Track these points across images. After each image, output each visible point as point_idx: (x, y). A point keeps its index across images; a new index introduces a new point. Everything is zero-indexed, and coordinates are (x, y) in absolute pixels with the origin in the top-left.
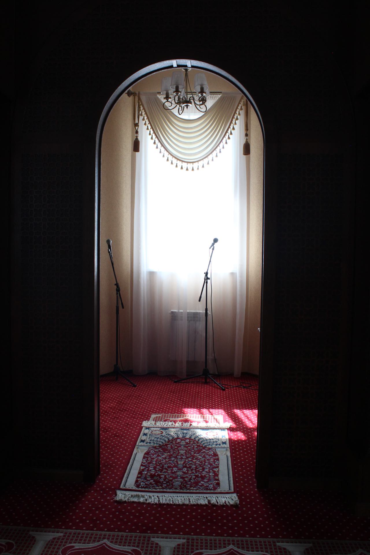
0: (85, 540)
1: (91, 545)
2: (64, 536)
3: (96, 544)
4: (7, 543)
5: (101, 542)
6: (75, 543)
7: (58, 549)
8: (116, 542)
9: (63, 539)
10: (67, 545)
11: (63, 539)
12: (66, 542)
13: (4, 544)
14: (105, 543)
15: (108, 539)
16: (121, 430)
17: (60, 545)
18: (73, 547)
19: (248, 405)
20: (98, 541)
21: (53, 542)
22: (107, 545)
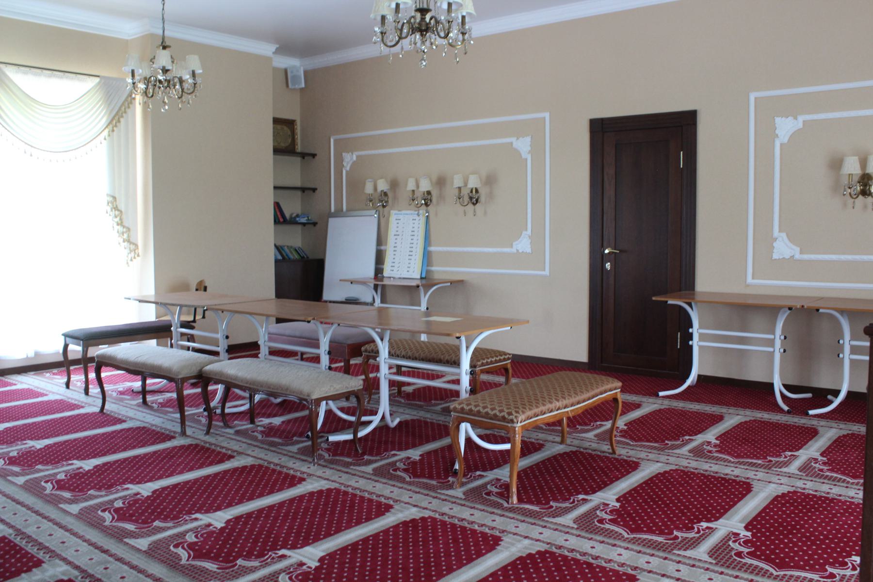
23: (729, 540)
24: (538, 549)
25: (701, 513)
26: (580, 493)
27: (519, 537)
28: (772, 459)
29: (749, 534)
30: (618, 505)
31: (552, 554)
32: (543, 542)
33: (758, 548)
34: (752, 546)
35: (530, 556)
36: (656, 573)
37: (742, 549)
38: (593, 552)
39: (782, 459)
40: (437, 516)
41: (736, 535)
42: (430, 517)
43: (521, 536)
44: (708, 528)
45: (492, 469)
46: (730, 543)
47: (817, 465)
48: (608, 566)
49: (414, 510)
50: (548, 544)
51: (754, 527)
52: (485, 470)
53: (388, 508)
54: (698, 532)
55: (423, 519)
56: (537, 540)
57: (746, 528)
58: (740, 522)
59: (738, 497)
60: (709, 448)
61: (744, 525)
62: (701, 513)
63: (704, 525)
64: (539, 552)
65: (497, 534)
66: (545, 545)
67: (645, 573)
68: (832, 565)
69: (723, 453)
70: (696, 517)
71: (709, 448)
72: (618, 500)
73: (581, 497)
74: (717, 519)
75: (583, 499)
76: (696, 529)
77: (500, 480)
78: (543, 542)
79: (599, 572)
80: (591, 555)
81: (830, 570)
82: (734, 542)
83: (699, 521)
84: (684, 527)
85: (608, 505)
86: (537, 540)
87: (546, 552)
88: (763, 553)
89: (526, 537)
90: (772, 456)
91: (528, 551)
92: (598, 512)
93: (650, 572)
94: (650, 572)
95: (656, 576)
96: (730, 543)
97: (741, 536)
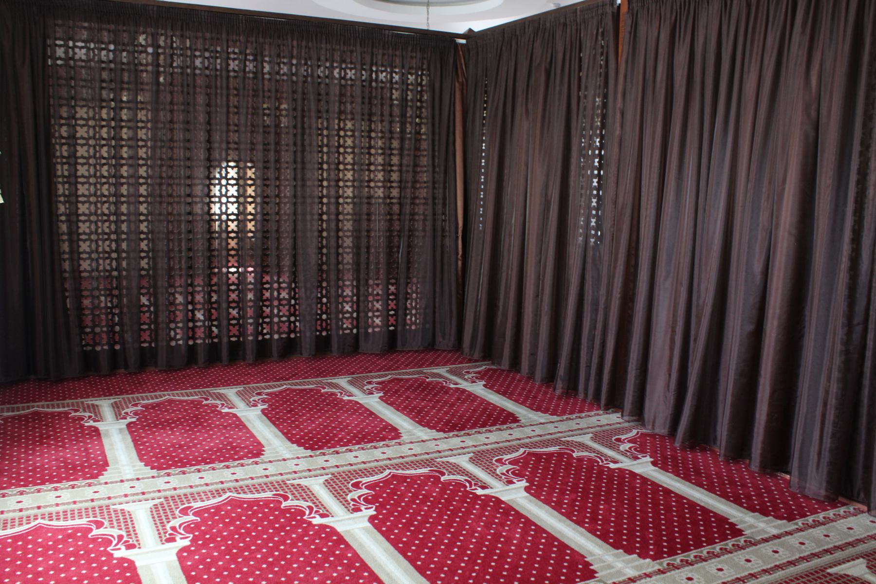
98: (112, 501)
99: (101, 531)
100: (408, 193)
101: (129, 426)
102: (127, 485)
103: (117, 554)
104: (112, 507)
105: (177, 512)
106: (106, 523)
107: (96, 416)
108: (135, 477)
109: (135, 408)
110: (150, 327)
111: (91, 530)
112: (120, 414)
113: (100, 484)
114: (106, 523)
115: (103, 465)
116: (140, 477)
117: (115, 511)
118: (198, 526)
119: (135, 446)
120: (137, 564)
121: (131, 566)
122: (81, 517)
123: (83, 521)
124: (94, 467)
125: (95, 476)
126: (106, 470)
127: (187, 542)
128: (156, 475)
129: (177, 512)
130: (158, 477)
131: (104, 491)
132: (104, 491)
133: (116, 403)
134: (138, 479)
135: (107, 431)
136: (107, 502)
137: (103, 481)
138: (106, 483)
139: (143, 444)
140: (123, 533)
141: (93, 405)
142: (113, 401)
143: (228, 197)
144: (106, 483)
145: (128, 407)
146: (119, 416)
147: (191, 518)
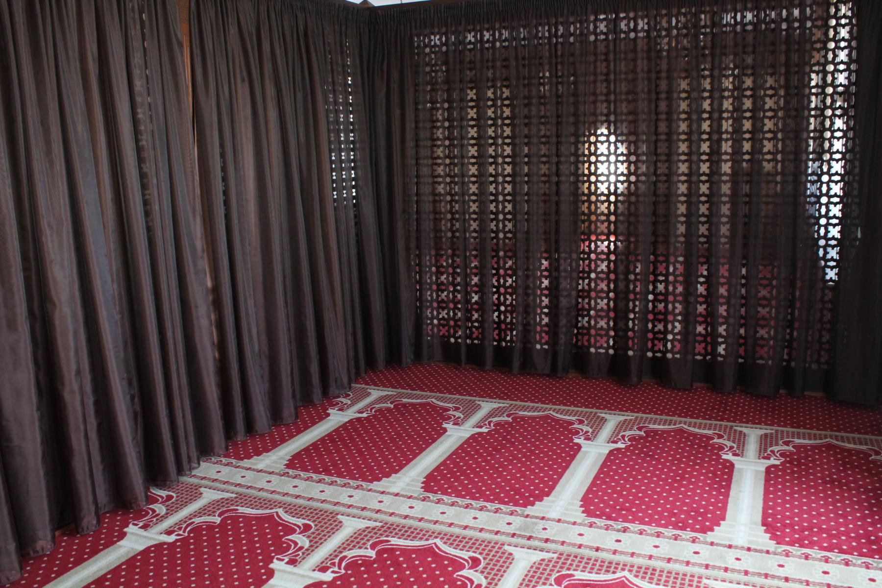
0: (458, 545)
1: (254, 512)
2: (559, 558)
3: (610, 576)
4: (305, 525)
5: (430, 542)
6: (575, 570)
7: (550, 575)
8: (644, 578)
9: (379, 530)
10: (564, 573)
11: (379, 530)
12: (381, 535)
13: (466, 558)
14: (435, 544)
15: (630, 571)
16: (562, 453)
17: (552, 571)
18: (572, 575)
19: (551, 478)
20: (427, 540)
21: (364, 531)
22: (437, 546)
23: (593, 432)
24: (381, 483)
25: (487, 441)
26: (365, 418)
27: (268, 470)
28: (506, 419)
29: (576, 441)
30: (445, 425)
31: (365, 479)
32: (375, 491)
33: (566, 429)
34: (571, 430)
35: (388, 475)
36: (403, 496)
37: (580, 426)
38: (473, 513)
39: (494, 420)
40: (234, 461)
41: (587, 439)
42: (242, 459)
43: (403, 496)
44: (481, 427)
45: (351, 421)
46: (591, 430)
47: (585, 428)
48: (482, 503)
49: (260, 466)
50: (370, 490)
51: (571, 448)
52: (359, 420)
53: (291, 464)
54: (490, 423)
55: (249, 457)
56: (383, 493)
57: (445, 430)
58: (586, 452)
59: (611, 461)
60: (457, 414)
61: (583, 449)
62: (487, 441)
63: (484, 430)
64: (379, 480)
65: (291, 472)
66: (374, 488)
67: (415, 495)
68: (641, 437)
69: (565, 421)
70: (492, 437)
71: (457, 414)
72: (445, 430)
73: (365, 415)
74: (473, 435)
75: (362, 413)
76: (626, 439)
77: (339, 410)
78: (375, 491)
79: (461, 491)
80: (351, 487)
81: (642, 433)
82: (587, 432)
83: (489, 433)
84: (503, 425)
85: (454, 424)
86: (383, 493)
87: (371, 481)
88: (561, 426)
89: (397, 495)
90: (507, 422)
91: (390, 479)
92: (349, 402)
93: (410, 497)
94: (410, 497)
95: (568, 520)
96: (591, 430)
97: (583, 438)
98: (709, 572)
99: (721, 441)
100: (662, 168)
101: (768, 470)
102: (733, 553)
103: (724, 457)
104: (705, 581)
105: (781, 442)
106: (726, 437)
107: (738, 448)
108: (746, 545)
109: (785, 448)
110: (733, 72)
111: (713, 439)
112: (765, 450)
113: (705, 543)
114: (726, 437)
115: (719, 517)
116: (752, 547)
117: (736, 431)
118: (792, 453)
119: (765, 485)
120: (736, 466)
121: (732, 465)
122: (710, 429)
123: (710, 432)
124: (706, 517)
125: (704, 530)
126: (719, 525)
127: (778, 463)
128: (771, 549)
129: (781, 442)
130: (775, 554)
131: (706, 554)
132: (706, 554)
133: (766, 435)
134: (749, 549)
135: (742, 469)
136: (702, 571)
137: (709, 540)
138: (712, 544)
139: (774, 485)
140: (735, 446)
141: (741, 432)
142: (763, 432)
143: (609, 165)
144: (712, 544)
145: (777, 444)
146: (763, 454)
147: (791, 448)
